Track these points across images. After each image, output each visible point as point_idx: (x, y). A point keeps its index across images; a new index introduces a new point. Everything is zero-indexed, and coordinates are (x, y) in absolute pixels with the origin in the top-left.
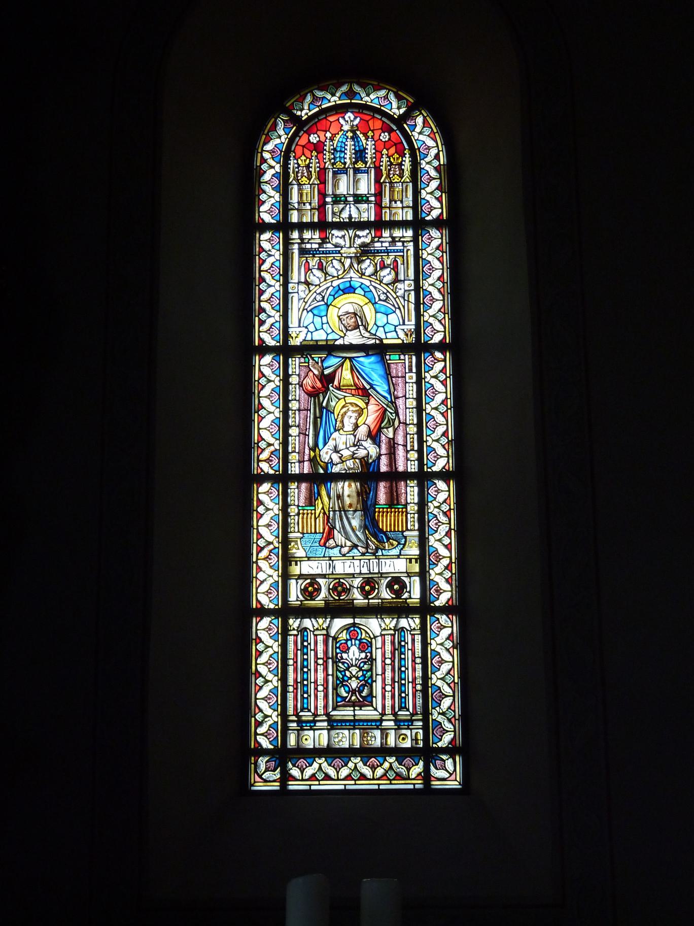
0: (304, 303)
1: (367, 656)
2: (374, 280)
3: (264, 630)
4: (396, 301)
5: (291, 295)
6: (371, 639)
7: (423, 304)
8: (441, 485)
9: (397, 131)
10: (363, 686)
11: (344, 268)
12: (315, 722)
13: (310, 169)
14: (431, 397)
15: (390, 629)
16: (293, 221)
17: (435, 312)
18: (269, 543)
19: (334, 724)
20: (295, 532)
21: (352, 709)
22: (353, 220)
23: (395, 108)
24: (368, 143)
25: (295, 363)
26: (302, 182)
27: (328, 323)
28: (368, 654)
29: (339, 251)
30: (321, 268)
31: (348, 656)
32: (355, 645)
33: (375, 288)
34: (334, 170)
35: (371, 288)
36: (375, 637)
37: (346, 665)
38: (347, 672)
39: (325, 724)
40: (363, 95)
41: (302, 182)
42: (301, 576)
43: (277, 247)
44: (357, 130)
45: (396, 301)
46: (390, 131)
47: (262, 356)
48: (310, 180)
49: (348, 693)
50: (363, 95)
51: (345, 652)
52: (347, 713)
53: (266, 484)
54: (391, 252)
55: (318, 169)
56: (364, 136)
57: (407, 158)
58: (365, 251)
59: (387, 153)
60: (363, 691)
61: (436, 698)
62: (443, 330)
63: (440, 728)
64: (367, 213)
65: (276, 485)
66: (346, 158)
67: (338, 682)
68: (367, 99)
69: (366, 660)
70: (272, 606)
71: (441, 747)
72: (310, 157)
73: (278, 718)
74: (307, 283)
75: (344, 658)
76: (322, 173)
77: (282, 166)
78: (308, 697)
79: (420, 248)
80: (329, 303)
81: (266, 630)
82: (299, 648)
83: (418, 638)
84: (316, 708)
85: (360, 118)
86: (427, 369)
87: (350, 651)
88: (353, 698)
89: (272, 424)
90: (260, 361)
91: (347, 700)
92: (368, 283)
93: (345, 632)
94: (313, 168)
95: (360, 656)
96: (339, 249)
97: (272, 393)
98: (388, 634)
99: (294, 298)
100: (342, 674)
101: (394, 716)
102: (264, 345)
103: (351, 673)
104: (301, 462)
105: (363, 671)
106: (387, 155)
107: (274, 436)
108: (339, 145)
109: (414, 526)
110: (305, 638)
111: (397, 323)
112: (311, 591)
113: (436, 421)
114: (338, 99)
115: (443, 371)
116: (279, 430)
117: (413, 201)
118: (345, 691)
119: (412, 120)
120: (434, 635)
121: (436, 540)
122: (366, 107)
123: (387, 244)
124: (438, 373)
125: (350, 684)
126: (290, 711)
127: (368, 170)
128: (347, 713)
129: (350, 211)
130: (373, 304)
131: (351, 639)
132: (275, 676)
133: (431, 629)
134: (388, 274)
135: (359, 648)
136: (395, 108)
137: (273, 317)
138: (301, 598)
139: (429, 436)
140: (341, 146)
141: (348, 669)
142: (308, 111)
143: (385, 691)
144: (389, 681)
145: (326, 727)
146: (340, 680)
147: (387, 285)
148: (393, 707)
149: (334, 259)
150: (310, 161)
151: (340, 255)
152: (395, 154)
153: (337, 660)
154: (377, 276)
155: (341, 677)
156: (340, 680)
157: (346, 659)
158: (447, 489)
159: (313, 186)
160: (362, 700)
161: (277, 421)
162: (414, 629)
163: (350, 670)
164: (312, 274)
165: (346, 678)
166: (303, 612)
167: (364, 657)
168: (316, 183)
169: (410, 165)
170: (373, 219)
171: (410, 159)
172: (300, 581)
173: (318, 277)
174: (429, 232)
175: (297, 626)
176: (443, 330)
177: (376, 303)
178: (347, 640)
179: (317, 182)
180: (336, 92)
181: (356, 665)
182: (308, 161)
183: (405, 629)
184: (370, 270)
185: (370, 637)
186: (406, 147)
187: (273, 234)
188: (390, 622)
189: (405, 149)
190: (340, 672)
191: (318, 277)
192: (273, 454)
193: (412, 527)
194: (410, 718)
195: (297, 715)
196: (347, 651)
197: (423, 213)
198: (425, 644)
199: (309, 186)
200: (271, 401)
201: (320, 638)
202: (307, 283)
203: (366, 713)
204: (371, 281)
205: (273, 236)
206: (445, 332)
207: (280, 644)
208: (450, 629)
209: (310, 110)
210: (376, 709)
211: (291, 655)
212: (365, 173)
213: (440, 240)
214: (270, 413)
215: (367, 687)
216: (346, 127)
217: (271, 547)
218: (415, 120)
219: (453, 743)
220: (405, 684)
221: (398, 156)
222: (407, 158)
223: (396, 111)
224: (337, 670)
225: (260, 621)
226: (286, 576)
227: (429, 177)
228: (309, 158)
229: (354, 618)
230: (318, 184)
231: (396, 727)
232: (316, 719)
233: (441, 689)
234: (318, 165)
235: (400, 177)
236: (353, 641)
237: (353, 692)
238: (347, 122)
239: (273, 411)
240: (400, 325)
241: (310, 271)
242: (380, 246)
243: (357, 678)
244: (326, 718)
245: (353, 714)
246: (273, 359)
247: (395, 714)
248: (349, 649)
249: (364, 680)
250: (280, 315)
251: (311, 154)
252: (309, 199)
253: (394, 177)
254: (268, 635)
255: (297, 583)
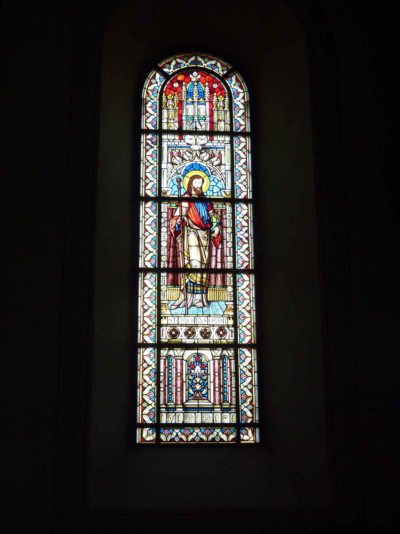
0: (171, 173)
1: (205, 372)
2: (209, 164)
3: (147, 375)
4: (221, 176)
5: (163, 170)
6: (207, 362)
7: (238, 282)
8: (245, 277)
9: (221, 83)
10: (204, 388)
11: (193, 156)
12: (175, 408)
13: (174, 101)
14: (244, 399)
15: (218, 356)
16: (164, 129)
17: (244, 251)
18: (149, 326)
19: (186, 409)
20: (164, 300)
21: (197, 401)
22: (197, 130)
23: (220, 70)
24: (205, 89)
25: (164, 207)
26: (169, 108)
27: (184, 187)
28: (206, 371)
29: (190, 147)
30: (179, 155)
31: (195, 372)
32: (199, 365)
33: (209, 168)
34: (187, 102)
35: (207, 167)
36: (209, 361)
37: (193, 376)
38: (194, 380)
39: (182, 410)
40: (203, 62)
41: (169, 108)
42: (167, 325)
43: (155, 95)
44: (200, 81)
45: (221, 176)
46: (218, 83)
47: (146, 203)
48: (174, 107)
49: (194, 392)
50: (203, 62)
51: (193, 369)
52: (193, 403)
53: (149, 202)
54: (218, 149)
55: (178, 102)
56: (203, 85)
57: (227, 98)
58: (204, 148)
59: (216, 94)
60: (203, 391)
61: (243, 398)
62: (245, 141)
63: (245, 415)
64: (205, 126)
65: (155, 204)
66: (194, 97)
67: (189, 386)
68: (205, 65)
69: (205, 374)
70: (153, 196)
71: (243, 269)
72: (174, 95)
73: (156, 290)
74: (173, 164)
75: (192, 372)
76: (180, 103)
77: (157, 306)
78: (172, 365)
79: (237, 286)
80: (184, 175)
81: (149, 298)
82: (167, 366)
83: (233, 362)
84: (176, 400)
85: (201, 75)
86: (243, 402)
87: (196, 368)
88: (198, 395)
89: (152, 240)
90: (145, 205)
91: (194, 396)
92: (205, 165)
93: (192, 358)
94: (176, 101)
95: (201, 372)
96: (190, 146)
97: (152, 241)
98: (217, 359)
99: (164, 172)
100: (191, 381)
101: (220, 406)
102: (145, 423)
103: (196, 381)
104: (168, 262)
105: (203, 380)
106: (216, 95)
107: (152, 360)
108: (190, 88)
109: (231, 284)
110: (170, 362)
111: (222, 188)
112: (174, 333)
113: (245, 355)
114: (189, 64)
115: (248, 249)
116: (156, 244)
117: (230, 121)
118: (193, 391)
119: (230, 77)
120: (242, 381)
121: (242, 308)
122: (204, 69)
123: (216, 144)
124: (242, 164)
125: (196, 387)
126: (162, 402)
127: (205, 103)
128: (193, 403)
129: (196, 125)
130: (208, 177)
131: (196, 362)
132: (155, 249)
133: (240, 358)
134: (216, 160)
135: (201, 367)
136: (220, 70)
137: (152, 179)
138: (168, 338)
139: (237, 147)
140: (191, 90)
141: (194, 379)
142: (173, 70)
143: (215, 391)
144: (217, 385)
145: (182, 412)
146: (190, 385)
147: (215, 166)
148: (220, 400)
149: (187, 151)
150: (174, 97)
151: (190, 149)
152: (221, 96)
153: (188, 374)
154: (210, 161)
155: (191, 383)
156: (190, 385)
157: (193, 373)
158: (247, 209)
159: (175, 110)
160: (202, 396)
161: (155, 119)
162: (231, 356)
163: (196, 379)
164: (175, 159)
165: (194, 384)
166: (171, 346)
167: (203, 372)
168: (177, 109)
169: (229, 102)
170: (208, 130)
171: (228, 98)
172: (168, 328)
173: (178, 161)
174: (239, 138)
175: (166, 354)
176: (245, 141)
177: (210, 176)
178: (194, 362)
179: (177, 108)
180: (188, 60)
181: (199, 377)
182: (173, 97)
183: (226, 357)
184: (206, 158)
185: (207, 361)
186: (227, 92)
187: (153, 135)
188: (218, 352)
189: (226, 93)
190: (190, 380)
191: (178, 161)
192: (151, 391)
193: (230, 284)
194: (229, 407)
195: (166, 405)
196: (194, 369)
197: (237, 212)
198: (237, 366)
199: (173, 110)
200: (152, 227)
201: (179, 361)
202: (173, 164)
203: (204, 403)
204: (207, 164)
205: (153, 137)
206: (251, 336)
207: (158, 146)
208: (245, 160)
209: (174, 70)
210: (210, 402)
211: (162, 370)
212: (204, 105)
213: (246, 193)
214: (151, 181)
215: (205, 389)
216: (193, 80)
217: (151, 328)
218: (231, 78)
219: (245, 130)
220: (226, 387)
221: (222, 97)
222: (227, 98)
223: (222, 73)
224: (188, 379)
225: (145, 350)
226: (159, 325)
227: (241, 190)
228: (173, 95)
229: (198, 350)
230: (178, 110)
231: (222, 412)
232: (176, 407)
233: (245, 372)
234: (178, 99)
235: (223, 107)
236: (198, 363)
237: (198, 391)
238: (194, 76)
239: (151, 306)
240: (223, 189)
241: (174, 157)
242: (212, 145)
243: (200, 384)
244: (182, 407)
245: (197, 404)
246: (152, 204)
247: (221, 404)
248: (195, 368)
249: (204, 385)
250: (156, 251)
251: (174, 94)
252: (173, 117)
253: (220, 108)
254: (149, 338)
255: (166, 329)
